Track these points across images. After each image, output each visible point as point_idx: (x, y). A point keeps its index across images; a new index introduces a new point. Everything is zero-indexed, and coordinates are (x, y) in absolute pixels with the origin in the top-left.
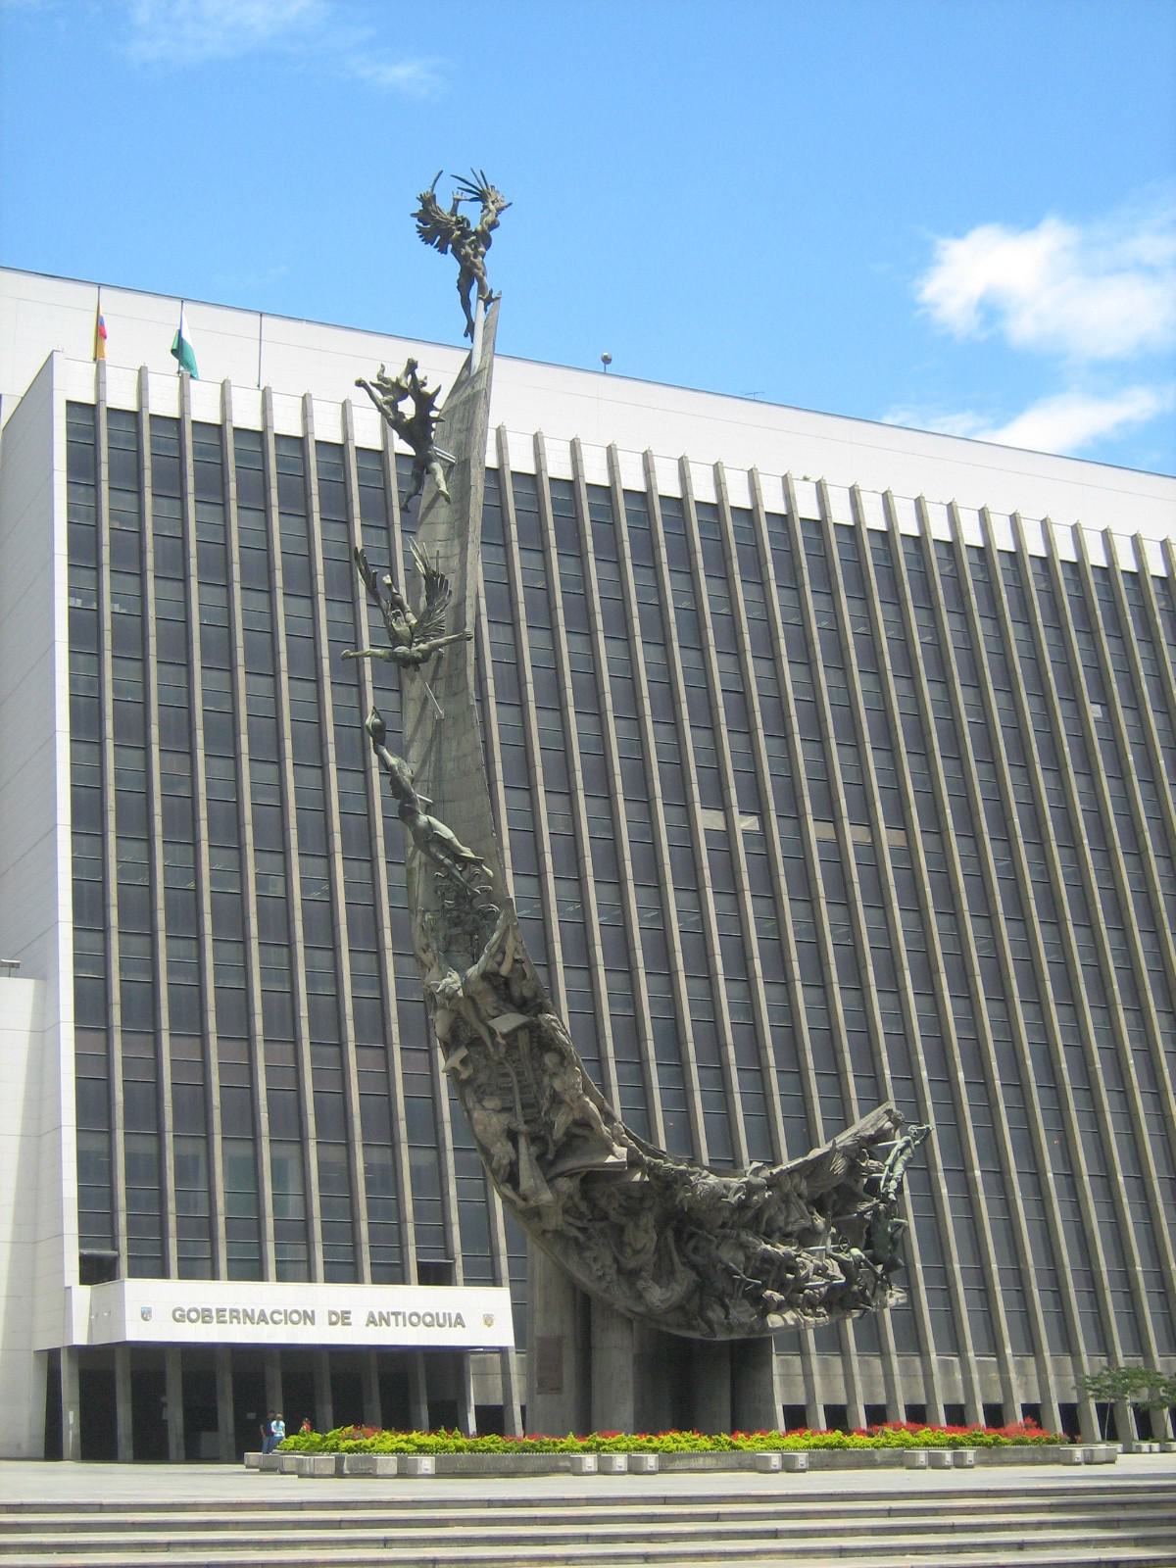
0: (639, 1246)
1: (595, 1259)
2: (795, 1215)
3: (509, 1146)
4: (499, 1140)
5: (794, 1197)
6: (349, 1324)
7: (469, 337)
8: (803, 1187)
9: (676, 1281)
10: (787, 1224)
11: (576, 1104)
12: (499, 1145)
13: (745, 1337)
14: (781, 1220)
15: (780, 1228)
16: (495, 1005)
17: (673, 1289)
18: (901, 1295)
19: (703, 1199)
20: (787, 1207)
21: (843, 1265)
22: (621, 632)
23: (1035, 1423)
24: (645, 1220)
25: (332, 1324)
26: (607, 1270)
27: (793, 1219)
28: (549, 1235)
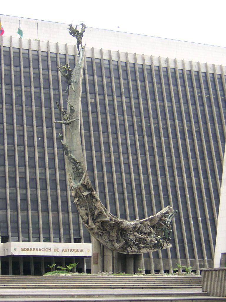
0: (113, 236)
6: (58, 251)
9: (121, 242)
10: (145, 231)
15: (144, 232)
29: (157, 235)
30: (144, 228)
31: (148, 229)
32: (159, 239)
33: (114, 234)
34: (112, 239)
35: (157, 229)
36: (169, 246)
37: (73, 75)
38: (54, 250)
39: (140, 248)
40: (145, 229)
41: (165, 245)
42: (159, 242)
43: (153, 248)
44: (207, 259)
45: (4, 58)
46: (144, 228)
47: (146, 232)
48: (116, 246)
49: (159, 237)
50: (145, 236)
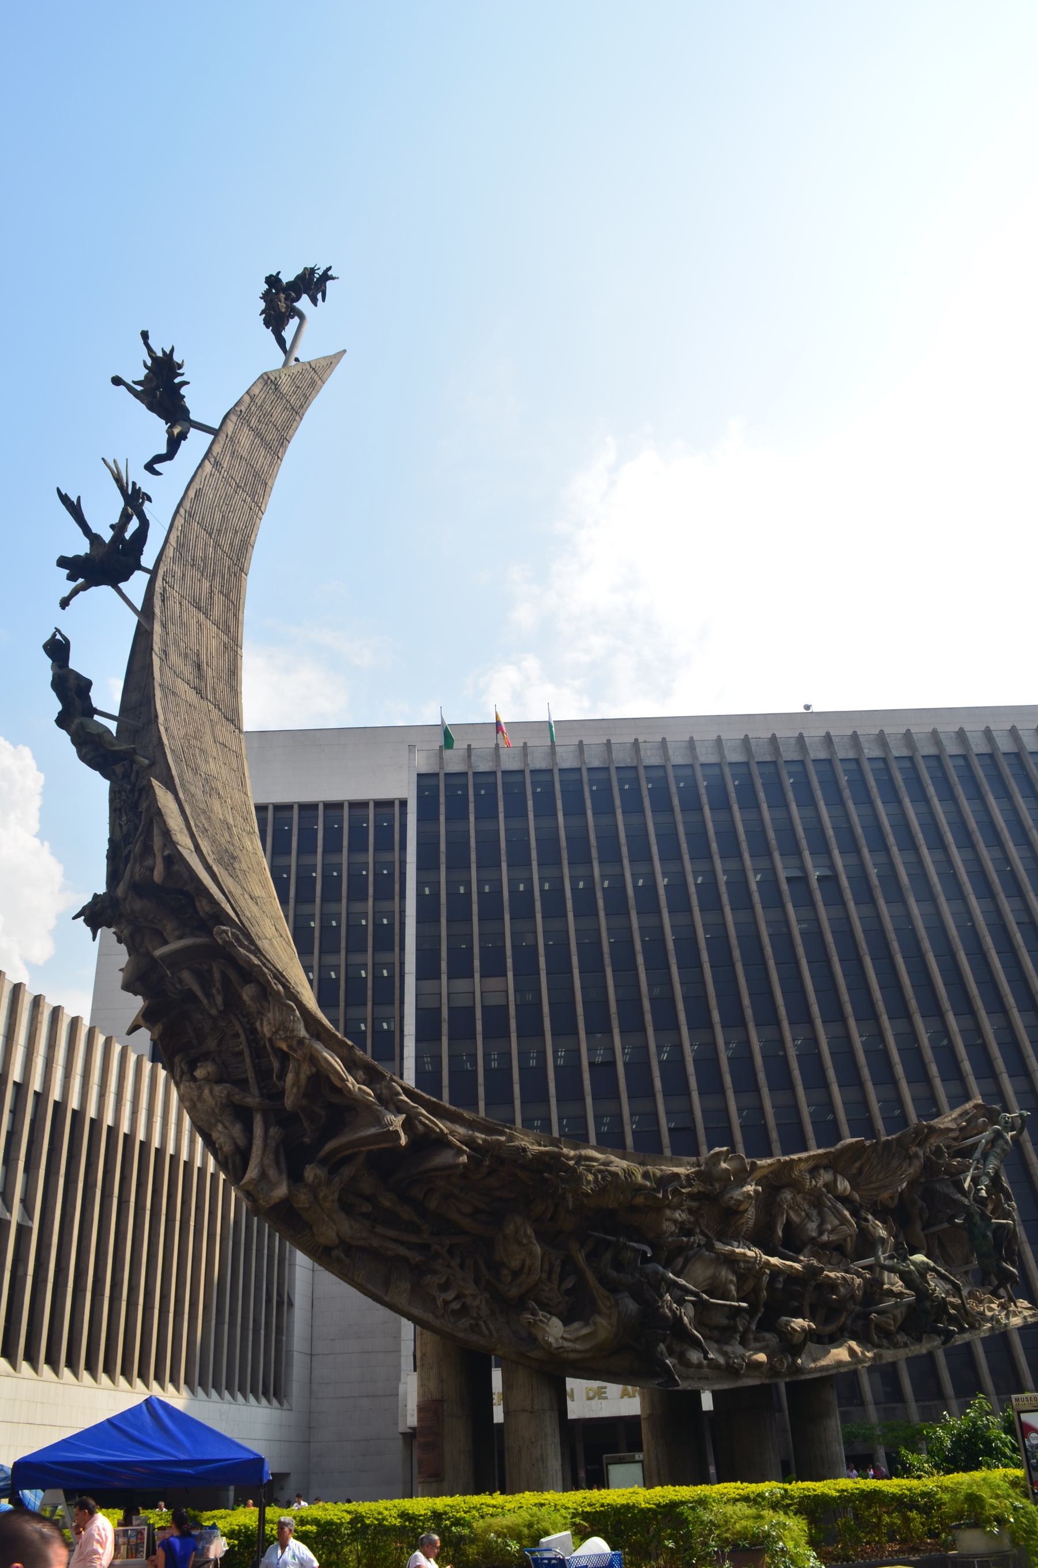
0: (515, 1264)
1: (445, 1287)
2: (833, 1221)
3: (237, 1130)
4: (218, 1121)
5: (829, 1200)
6: (606, 1398)
7: (330, 273)
8: (843, 1185)
9: (600, 1313)
10: (821, 1233)
11: (300, 1052)
12: (220, 1127)
13: (767, 1381)
14: (812, 1227)
15: (813, 1240)
16: (177, 933)
17: (595, 1324)
18: (1031, 1312)
19: (531, 1160)
20: (821, 1214)
21: (904, 1276)
22: (933, 1010)
23: (304, 303)
24: (512, 1227)
25: (589, 1399)
26: (469, 1301)
27: (829, 1227)
28: (335, 1253)
29: (902, 1252)
30: (815, 1213)
31: (844, 1221)
32: (923, 1276)
33: (526, 1249)
34: (514, 1292)
35: (923, 1229)
36: (1015, 1315)
37: (186, 383)
38: (587, 1393)
39: (791, 1345)
40: (822, 1222)
41: (993, 1308)
42: (923, 1294)
43: (902, 1338)
44: (771, 1155)
45: (752, 1002)
46: (808, 1215)
47: (825, 1237)
48: (551, 1340)
49: (919, 1258)
50: (815, 1262)
